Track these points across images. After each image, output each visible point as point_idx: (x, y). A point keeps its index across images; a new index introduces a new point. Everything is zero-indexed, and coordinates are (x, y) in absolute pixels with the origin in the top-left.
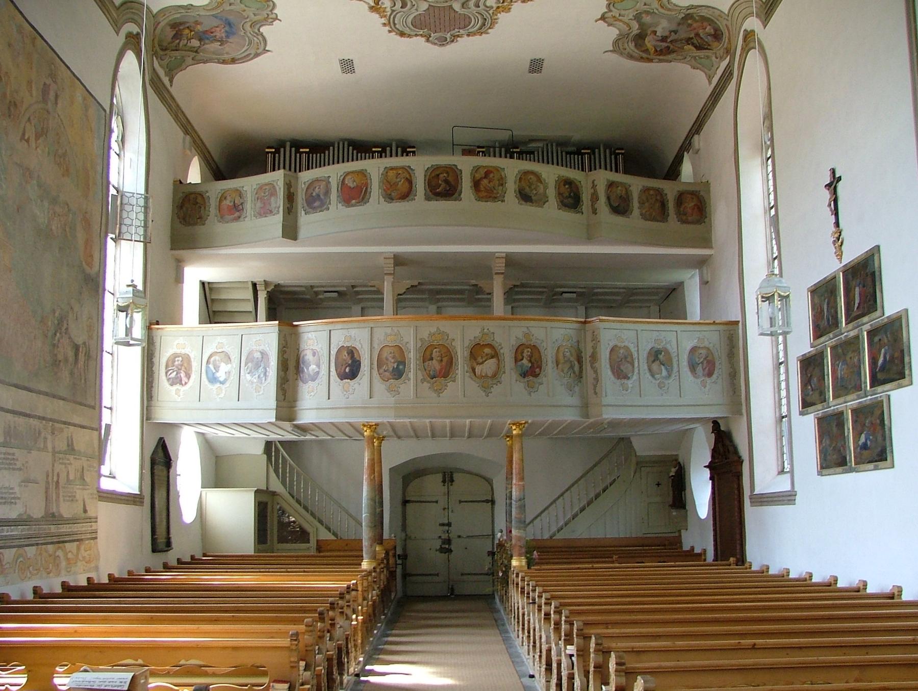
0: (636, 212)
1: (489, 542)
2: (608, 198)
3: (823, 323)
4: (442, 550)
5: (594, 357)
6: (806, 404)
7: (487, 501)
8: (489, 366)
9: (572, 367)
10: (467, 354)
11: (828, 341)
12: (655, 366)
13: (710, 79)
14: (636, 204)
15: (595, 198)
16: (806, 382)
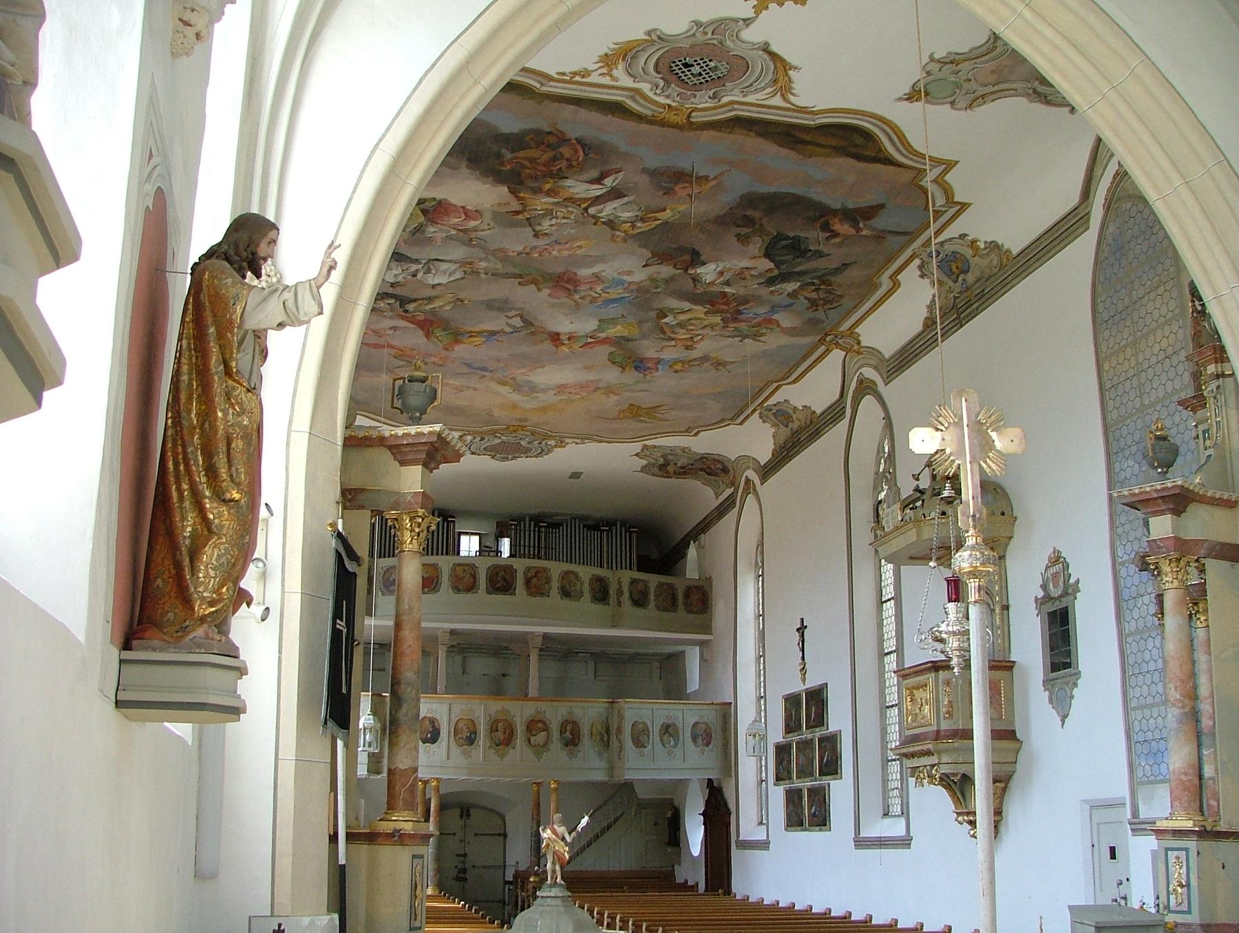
0: (652, 604)
1: (500, 872)
2: (631, 594)
3: (791, 726)
4: (458, 879)
5: (619, 730)
6: (779, 779)
7: (500, 835)
8: (540, 738)
9: (602, 739)
10: (524, 728)
11: (795, 738)
12: (666, 737)
13: (717, 495)
14: (652, 597)
15: (620, 592)
16: (779, 762)
